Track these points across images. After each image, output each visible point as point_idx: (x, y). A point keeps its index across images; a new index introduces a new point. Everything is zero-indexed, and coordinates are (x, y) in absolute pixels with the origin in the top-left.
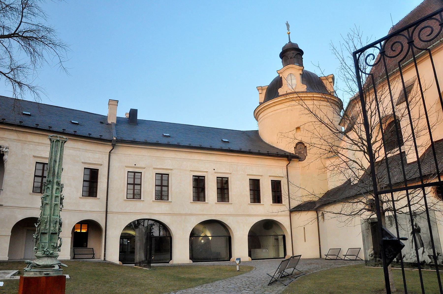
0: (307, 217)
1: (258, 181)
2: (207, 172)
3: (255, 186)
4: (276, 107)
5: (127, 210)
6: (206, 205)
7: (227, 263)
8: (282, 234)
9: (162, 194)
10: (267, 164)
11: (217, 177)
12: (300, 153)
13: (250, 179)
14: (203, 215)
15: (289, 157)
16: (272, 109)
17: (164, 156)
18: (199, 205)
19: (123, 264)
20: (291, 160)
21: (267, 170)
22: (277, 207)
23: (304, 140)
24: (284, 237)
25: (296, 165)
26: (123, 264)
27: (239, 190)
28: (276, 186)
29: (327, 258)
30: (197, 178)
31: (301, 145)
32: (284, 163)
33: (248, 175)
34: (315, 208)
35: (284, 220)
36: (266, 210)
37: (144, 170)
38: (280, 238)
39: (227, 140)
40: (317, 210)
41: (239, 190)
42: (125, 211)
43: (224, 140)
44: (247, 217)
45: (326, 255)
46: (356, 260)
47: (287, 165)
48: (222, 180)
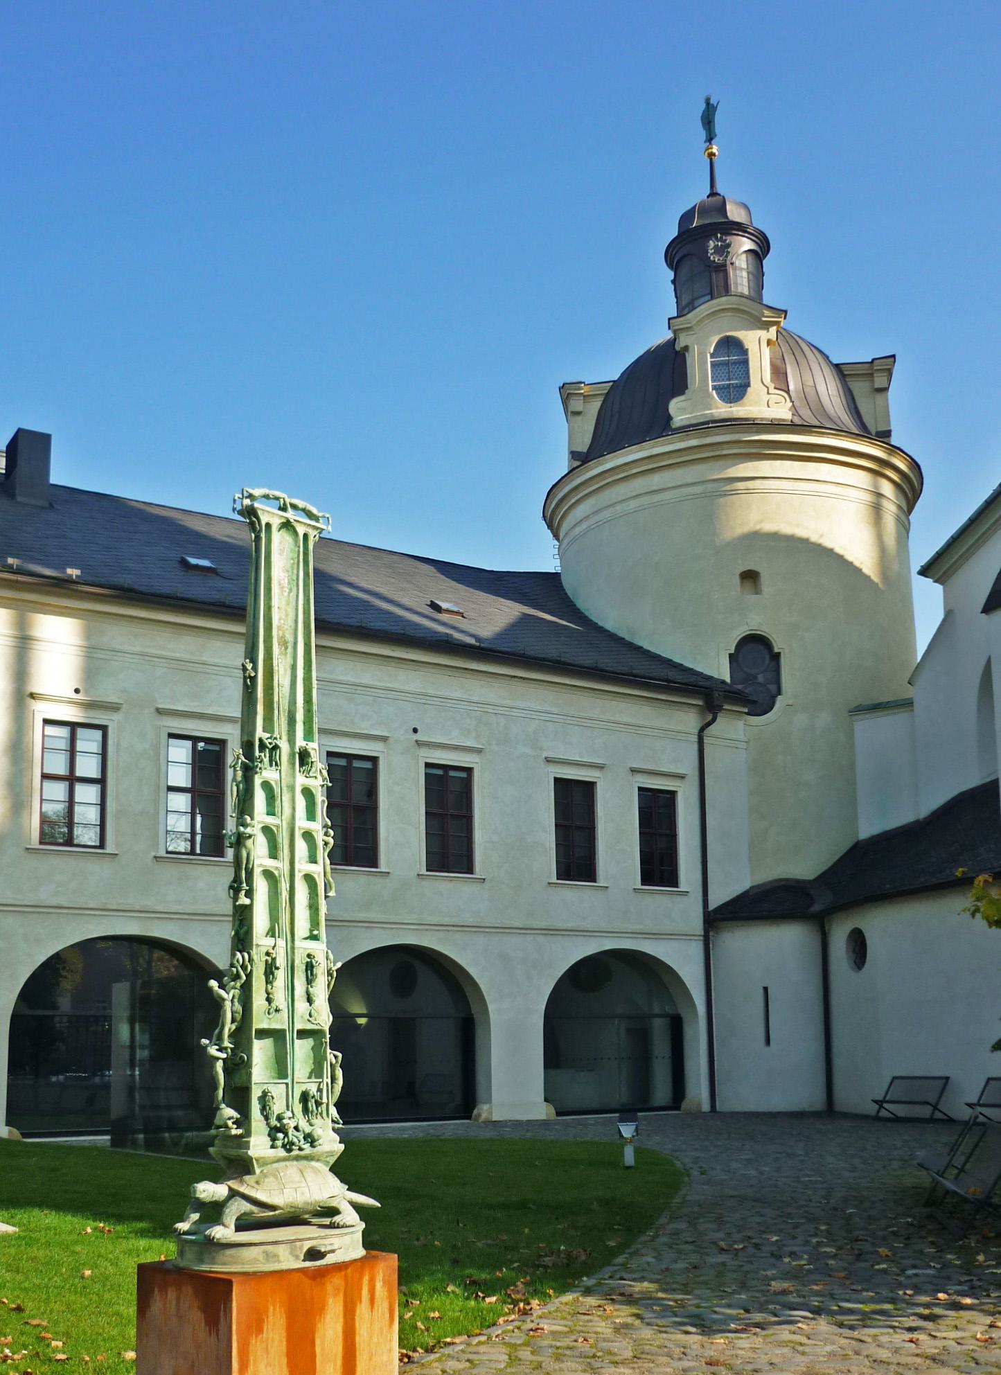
0: (775, 949)
1: (588, 788)
2: (384, 739)
3: (575, 804)
4: (657, 480)
5: (44, 895)
6: (678, 899)
7: (452, 1128)
8: (668, 1009)
9: (450, 846)
10: (624, 719)
11: (428, 765)
12: (750, 679)
13: (556, 779)
14: (79, 911)
15: (709, 697)
16: (640, 484)
17: (205, 658)
18: (575, 894)
19: (24, 1135)
20: (720, 708)
21: (624, 743)
22: (658, 900)
23: (766, 630)
24: (676, 1027)
25: (733, 728)
26: (24, 1135)
27: (515, 822)
28: (657, 811)
29: (884, 1113)
30: (343, 762)
31: (756, 651)
32: (687, 720)
33: (548, 760)
34: (817, 907)
35: (685, 961)
36: (618, 911)
37: (116, 717)
38: (659, 1028)
39: (205, 563)
40: (821, 923)
41: (515, 822)
42: (31, 899)
43: (193, 561)
44: (541, 939)
45: (880, 1103)
46: (931, 1120)
47: (702, 730)
48: (348, 769)
